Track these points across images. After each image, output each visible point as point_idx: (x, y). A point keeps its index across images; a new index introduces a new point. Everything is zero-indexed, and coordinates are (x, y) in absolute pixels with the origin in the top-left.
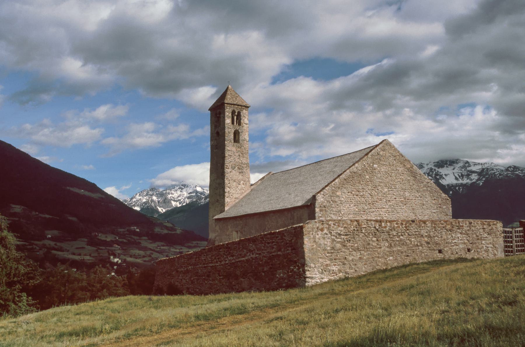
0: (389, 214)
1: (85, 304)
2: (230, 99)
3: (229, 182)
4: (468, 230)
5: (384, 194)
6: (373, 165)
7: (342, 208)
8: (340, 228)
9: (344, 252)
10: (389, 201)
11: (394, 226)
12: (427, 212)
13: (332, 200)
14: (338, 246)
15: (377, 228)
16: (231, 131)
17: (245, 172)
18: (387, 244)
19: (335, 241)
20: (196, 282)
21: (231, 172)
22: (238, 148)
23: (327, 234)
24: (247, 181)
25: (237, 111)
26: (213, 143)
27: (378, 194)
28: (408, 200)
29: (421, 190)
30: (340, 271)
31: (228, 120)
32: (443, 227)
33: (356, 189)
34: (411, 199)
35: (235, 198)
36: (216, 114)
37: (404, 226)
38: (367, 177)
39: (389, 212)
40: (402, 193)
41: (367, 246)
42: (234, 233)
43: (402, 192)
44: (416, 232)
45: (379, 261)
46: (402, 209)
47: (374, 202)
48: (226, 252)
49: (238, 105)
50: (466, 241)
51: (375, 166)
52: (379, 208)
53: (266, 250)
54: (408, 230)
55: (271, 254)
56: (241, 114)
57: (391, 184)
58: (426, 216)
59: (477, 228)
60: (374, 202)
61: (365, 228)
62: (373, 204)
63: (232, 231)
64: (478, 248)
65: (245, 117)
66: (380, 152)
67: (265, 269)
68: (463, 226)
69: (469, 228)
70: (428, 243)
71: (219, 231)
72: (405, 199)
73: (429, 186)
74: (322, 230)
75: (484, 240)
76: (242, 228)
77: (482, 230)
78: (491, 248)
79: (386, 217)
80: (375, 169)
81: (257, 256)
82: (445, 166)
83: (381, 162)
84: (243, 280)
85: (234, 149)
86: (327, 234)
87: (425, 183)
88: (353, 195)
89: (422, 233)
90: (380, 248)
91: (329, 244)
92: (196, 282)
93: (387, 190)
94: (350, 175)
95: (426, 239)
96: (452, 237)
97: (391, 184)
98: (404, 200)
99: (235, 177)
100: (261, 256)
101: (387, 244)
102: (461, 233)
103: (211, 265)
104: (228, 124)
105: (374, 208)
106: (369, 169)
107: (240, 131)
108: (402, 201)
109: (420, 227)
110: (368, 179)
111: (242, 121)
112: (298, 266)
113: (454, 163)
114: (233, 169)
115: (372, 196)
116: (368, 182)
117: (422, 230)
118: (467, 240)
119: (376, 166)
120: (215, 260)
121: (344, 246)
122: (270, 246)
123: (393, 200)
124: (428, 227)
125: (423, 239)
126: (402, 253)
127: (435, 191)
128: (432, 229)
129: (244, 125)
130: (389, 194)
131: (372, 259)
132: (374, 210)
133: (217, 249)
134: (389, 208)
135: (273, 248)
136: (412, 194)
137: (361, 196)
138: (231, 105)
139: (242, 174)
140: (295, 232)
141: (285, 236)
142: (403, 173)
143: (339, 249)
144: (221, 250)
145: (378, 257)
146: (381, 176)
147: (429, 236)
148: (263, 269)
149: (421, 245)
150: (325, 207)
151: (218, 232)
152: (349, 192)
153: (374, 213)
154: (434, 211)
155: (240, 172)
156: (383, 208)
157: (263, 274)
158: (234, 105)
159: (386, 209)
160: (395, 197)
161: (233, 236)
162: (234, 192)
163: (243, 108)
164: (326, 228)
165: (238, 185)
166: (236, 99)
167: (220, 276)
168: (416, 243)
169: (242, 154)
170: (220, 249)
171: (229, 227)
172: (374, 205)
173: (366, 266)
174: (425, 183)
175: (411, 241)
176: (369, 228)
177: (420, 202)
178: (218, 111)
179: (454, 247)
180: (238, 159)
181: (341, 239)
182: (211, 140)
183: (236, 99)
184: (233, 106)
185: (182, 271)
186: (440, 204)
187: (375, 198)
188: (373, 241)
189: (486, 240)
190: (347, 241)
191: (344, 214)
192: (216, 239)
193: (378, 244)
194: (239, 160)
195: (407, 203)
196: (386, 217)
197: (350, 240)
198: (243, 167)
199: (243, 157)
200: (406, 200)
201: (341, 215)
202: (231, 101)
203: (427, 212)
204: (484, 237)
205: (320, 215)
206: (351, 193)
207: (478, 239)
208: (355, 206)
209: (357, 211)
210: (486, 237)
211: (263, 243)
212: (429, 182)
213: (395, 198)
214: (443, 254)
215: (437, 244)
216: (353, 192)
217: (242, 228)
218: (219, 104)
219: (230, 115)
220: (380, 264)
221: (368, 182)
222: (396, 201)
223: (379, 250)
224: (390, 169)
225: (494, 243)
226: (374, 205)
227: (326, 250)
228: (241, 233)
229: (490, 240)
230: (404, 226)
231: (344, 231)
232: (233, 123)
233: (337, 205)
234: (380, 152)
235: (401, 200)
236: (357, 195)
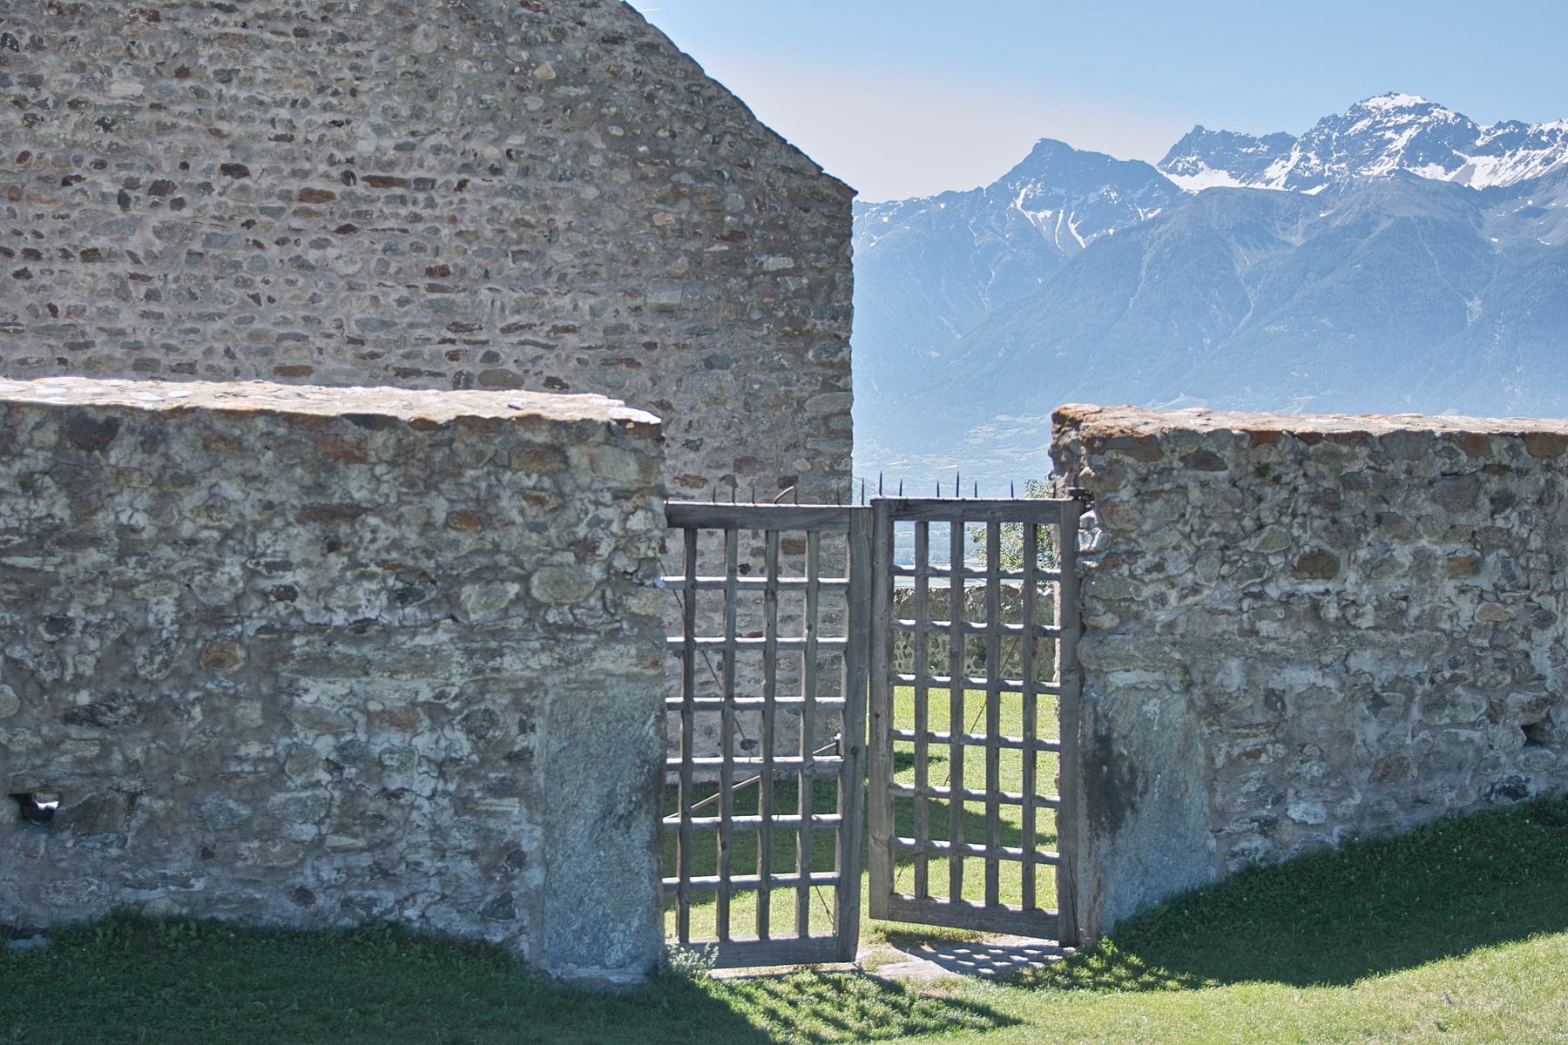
0: (154, 307)
1: (1509, 951)
28: (382, 193)
34: (421, 184)
43: (320, 118)
58: (571, 339)
72: (348, 177)
75: (320, 665)
77: (304, 534)
87: (574, 47)
93: (136, 88)
98: (338, 189)
136: (432, 140)
156: (90, 255)
159: (124, 267)
189: (365, 667)
204: (330, 634)
225: (499, 701)
229: (420, 663)
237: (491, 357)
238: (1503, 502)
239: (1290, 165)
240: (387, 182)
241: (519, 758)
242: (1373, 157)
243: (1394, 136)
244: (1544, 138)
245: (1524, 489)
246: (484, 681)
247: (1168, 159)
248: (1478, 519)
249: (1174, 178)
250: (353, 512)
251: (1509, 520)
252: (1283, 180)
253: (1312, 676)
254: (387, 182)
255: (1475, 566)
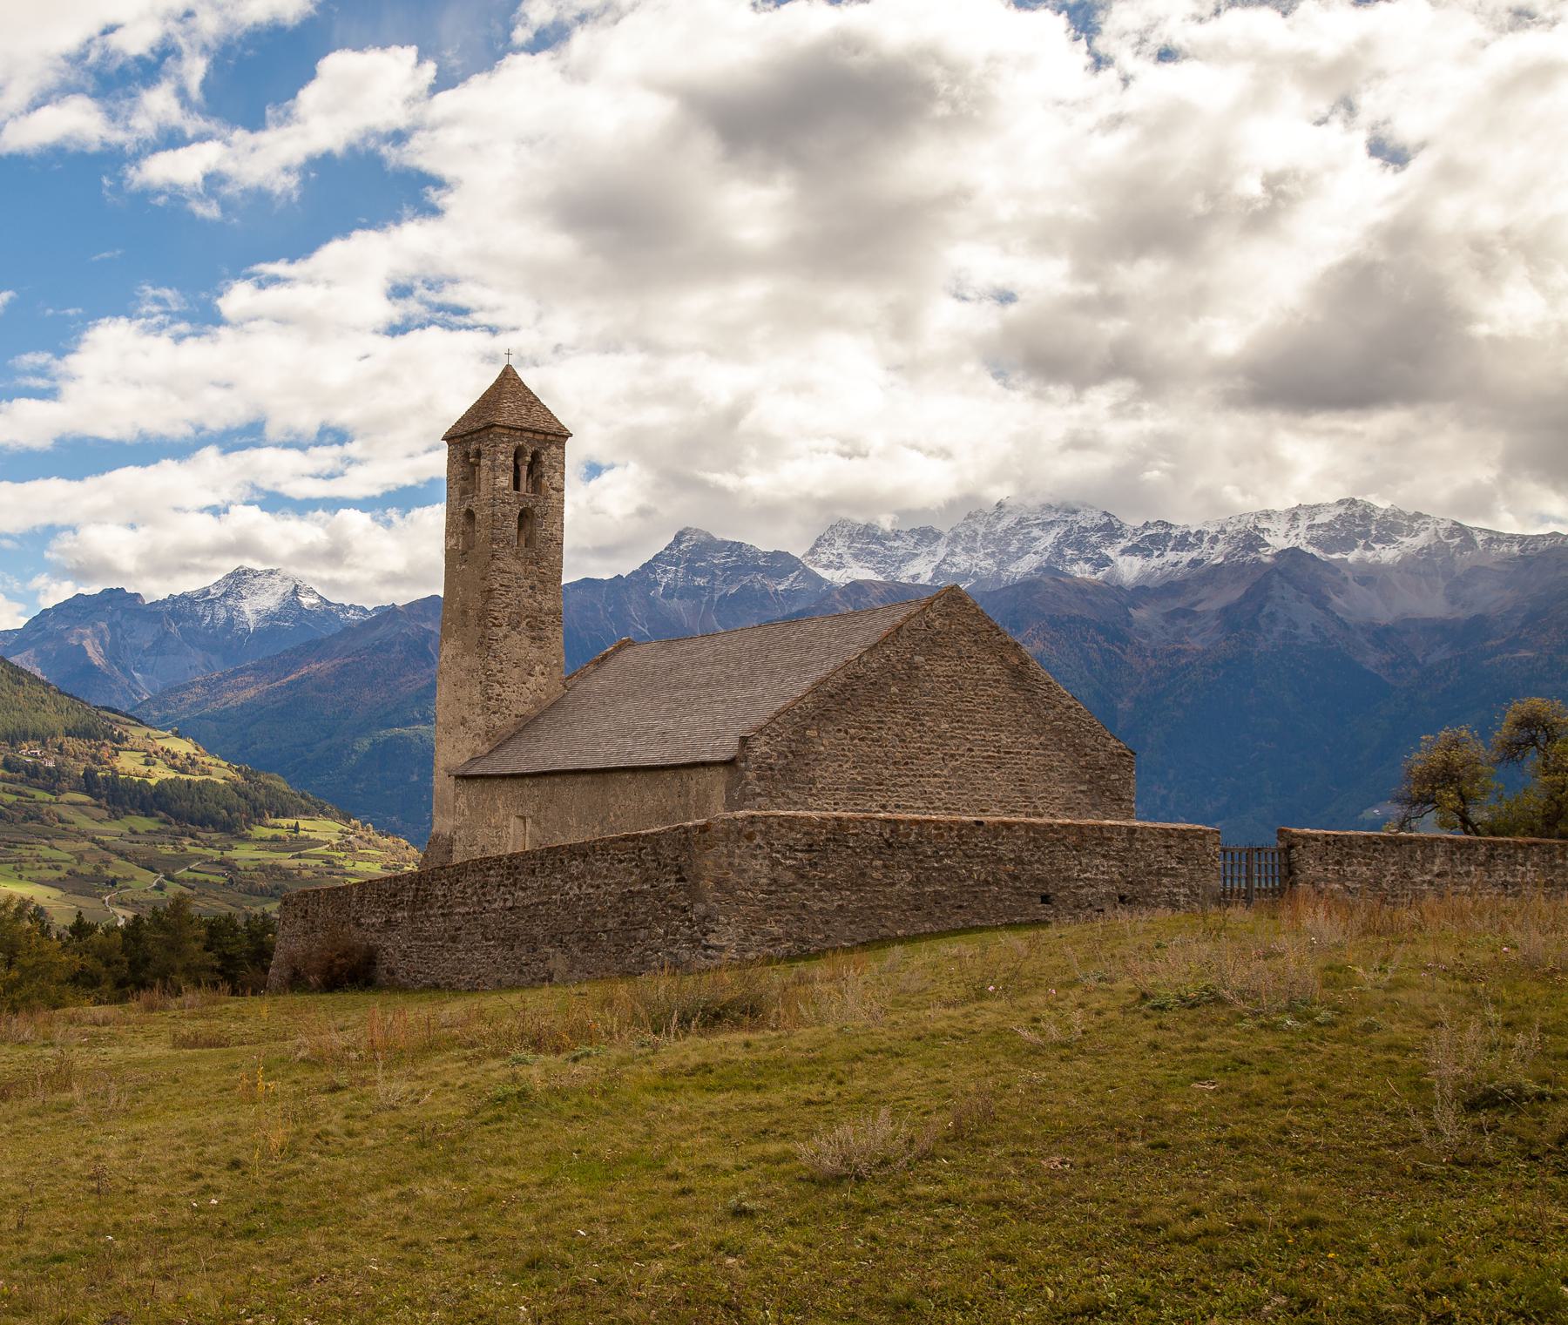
2: (511, 415)
3: (499, 667)
4: (1125, 850)
5: (940, 737)
6: (912, 658)
7: (818, 773)
8: (793, 835)
9: (802, 891)
10: (952, 756)
11: (929, 834)
12: (1061, 790)
13: (792, 752)
14: (789, 877)
15: (887, 836)
16: (511, 510)
17: (548, 638)
18: (908, 876)
19: (781, 864)
20: (415, 956)
21: (506, 637)
22: (531, 563)
23: (761, 847)
24: (555, 665)
25: (530, 450)
26: (453, 542)
27: (921, 737)
29: (1048, 727)
30: (788, 935)
31: (502, 479)
32: (1058, 840)
33: (860, 722)
34: (1018, 753)
35: (517, 716)
36: (467, 455)
37: (954, 833)
38: (894, 689)
39: (949, 788)
40: (990, 736)
41: (858, 880)
42: (513, 821)
44: (985, 848)
45: (887, 918)
46: (987, 779)
47: (909, 758)
48: (508, 879)
49: (535, 432)
50: (1117, 876)
51: (917, 658)
52: (921, 776)
53: (613, 878)
54: (966, 843)
55: (625, 887)
56: (543, 458)
57: (959, 710)
59: (1150, 845)
60: (909, 758)
61: (856, 835)
62: (907, 763)
63: (507, 817)
64: (1149, 896)
65: (554, 468)
66: (933, 620)
67: (610, 925)
68: (1110, 839)
69: (1126, 845)
70: (1015, 878)
71: (467, 812)
72: (998, 752)
73: (1070, 718)
74: (750, 837)
76: (539, 810)
78: (1185, 896)
79: (940, 800)
80: (917, 668)
81: (591, 890)
82: (1361, 542)
83: (938, 650)
84: (551, 950)
85: (517, 568)
86: (761, 847)
87: (1060, 709)
88: (852, 738)
89: (999, 853)
90: (893, 884)
91: (765, 870)
92: (415, 956)
94: (845, 685)
95: (1010, 867)
96: (1080, 864)
97: (959, 710)
99: (519, 653)
100: (601, 891)
101: (908, 876)
102: (1104, 856)
103: (462, 910)
104: (504, 489)
105: (908, 776)
106: (899, 667)
107: (537, 510)
108: (989, 757)
109: (996, 838)
110: (894, 694)
111: (545, 481)
112: (690, 920)
113: (1400, 533)
114: (514, 629)
115: (904, 741)
116: (896, 702)
117: (1001, 844)
118: (1120, 874)
119: (922, 659)
120: (475, 899)
121: (803, 876)
122: (624, 869)
123: (963, 755)
124: (1018, 838)
125: (1001, 867)
126: (946, 898)
127: (1089, 731)
128: (1027, 843)
129: (552, 492)
130: (952, 737)
131: (869, 912)
132: (907, 780)
133: (481, 870)
134: (950, 777)
135: (631, 874)
137: (873, 740)
138: (512, 432)
139: (538, 643)
140: (687, 839)
141: (661, 847)
142: (997, 681)
143: (790, 885)
144: (492, 872)
145: (886, 907)
146: (933, 688)
147: (1019, 861)
148: (605, 925)
149: (997, 882)
150: (771, 769)
151: (463, 815)
152: (839, 730)
153: (906, 789)
154: (1084, 788)
155: (534, 638)
156: (935, 776)
157: (605, 937)
158: (523, 430)
160: (968, 746)
161: (511, 830)
162: (514, 697)
163: (551, 442)
164: (761, 831)
165: (526, 677)
166: (529, 410)
167: (488, 940)
168: (983, 876)
169: (542, 582)
170: (489, 869)
171: (499, 803)
172: (910, 766)
173: (853, 927)
174: (1060, 709)
175: (970, 871)
176: (865, 837)
177: (1042, 760)
178: (474, 446)
179: (1084, 891)
180: (530, 596)
181: (795, 859)
182: (449, 534)
183: (529, 410)
184: (518, 434)
185: (373, 925)
186: (1102, 769)
187: (913, 748)
188: (876, 869)
190: (810, 865)
191: (823, 788)
192: (456, 837)
193: (885, 877)
194: (531, 601)
195: (1004, 764)
196: (940, 800)
197: (816, 863)
198: (543, 622)
199: (546, 593)
200: (1002, 755)
201: (814, 791)
202: (515, 421)
203: (1061, 790)
205: (758, 790)
206: (846, 732)
207: (1149, 873)
208: (855, 767)
209: (859, 783)
210: (1172, 868)
211: (606, 860)
212: (1071, 707)
213: (970, 750)
214: (1054, 907)
215: (1039, 881)
216: (852, 731)
217: (539, 810)
218: (475, 425)
219: (510, 461)
220: (888, 924)
221: (896, 702)
222: (972, 757)
223: (888, 890)
224: (959, 668)
225: (1193, 883)
226: (910, 766)
227: (757, 884)
228: (537, 823)
229: (1183, 876)
230: (954, 833)
231: (804, 841)
232: (517, 487)
233: (807, 764)
234: (933, 620)
235: (985, 754)
236: (862, 739)
237: (1036, 807)
238: (1375, 850)
239: (937, 560)
240: (1009, 753)
241: (1197, 895)
242: (1022, 552)
243: (1041, 533)
244: (1191, 539)
245: (1380, 847)
246: (1191, 879)
247: (812, 552)
248: (1369, 854)
249: (820, 571)
250: (1171, 847)
251: (1376, 855)
252: (930, 575)
253: (1337, 886)
254: (1009, 753)
255: (1369, 864)
